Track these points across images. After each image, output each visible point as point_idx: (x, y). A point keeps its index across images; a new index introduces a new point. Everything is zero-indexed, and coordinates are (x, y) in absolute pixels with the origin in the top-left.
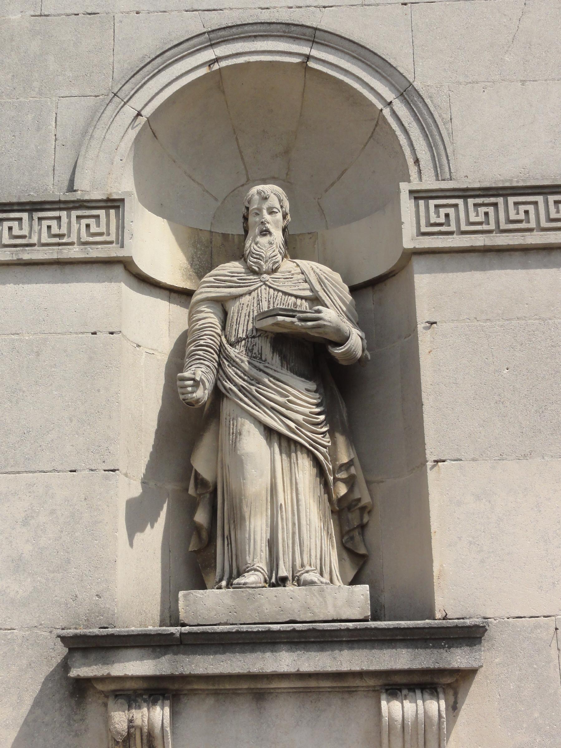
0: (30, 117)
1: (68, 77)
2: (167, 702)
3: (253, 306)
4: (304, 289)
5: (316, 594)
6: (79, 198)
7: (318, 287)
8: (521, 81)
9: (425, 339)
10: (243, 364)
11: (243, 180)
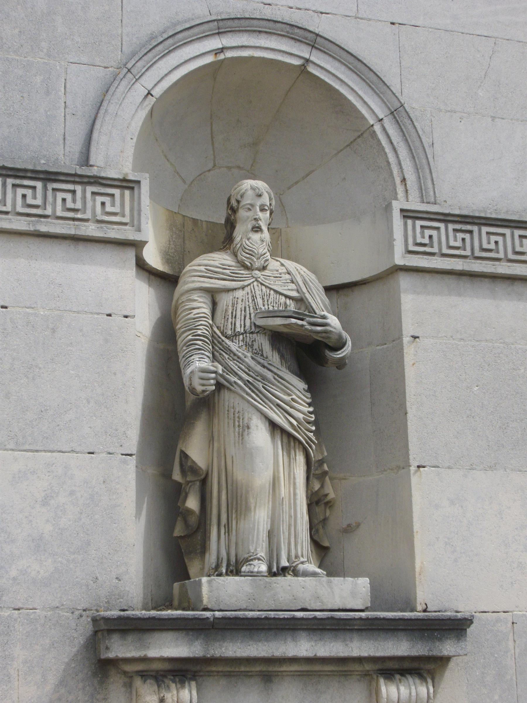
0: (39, 79)
1: (77, 43)
2: (193, 683)
3: (248, 302)
4: (292, 290)
5: (325, 585)
6: (95, 174)
7: (304, 290)
8: (492, 117)
9: (410, 353)
10: (246, 360)
11: (210, 165)
